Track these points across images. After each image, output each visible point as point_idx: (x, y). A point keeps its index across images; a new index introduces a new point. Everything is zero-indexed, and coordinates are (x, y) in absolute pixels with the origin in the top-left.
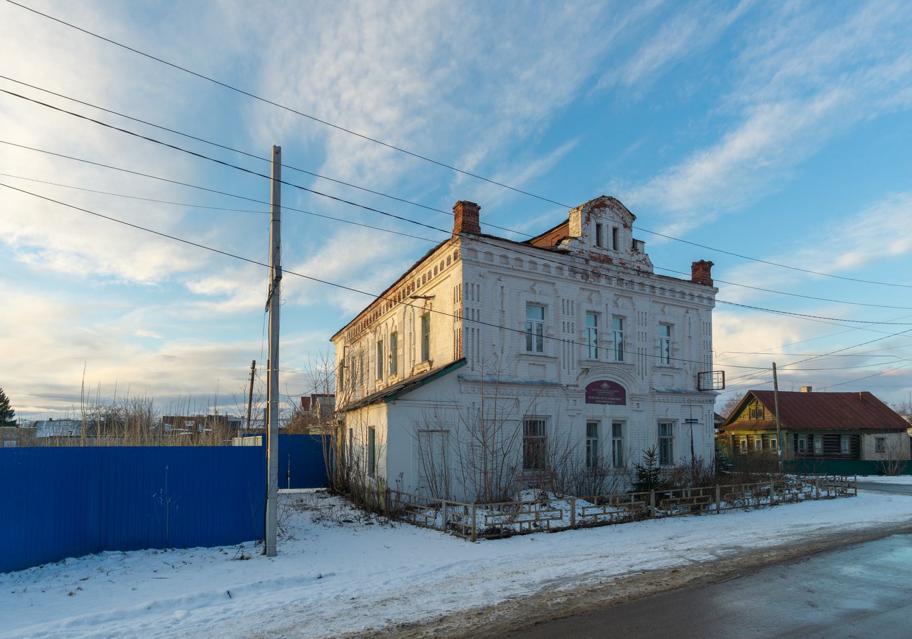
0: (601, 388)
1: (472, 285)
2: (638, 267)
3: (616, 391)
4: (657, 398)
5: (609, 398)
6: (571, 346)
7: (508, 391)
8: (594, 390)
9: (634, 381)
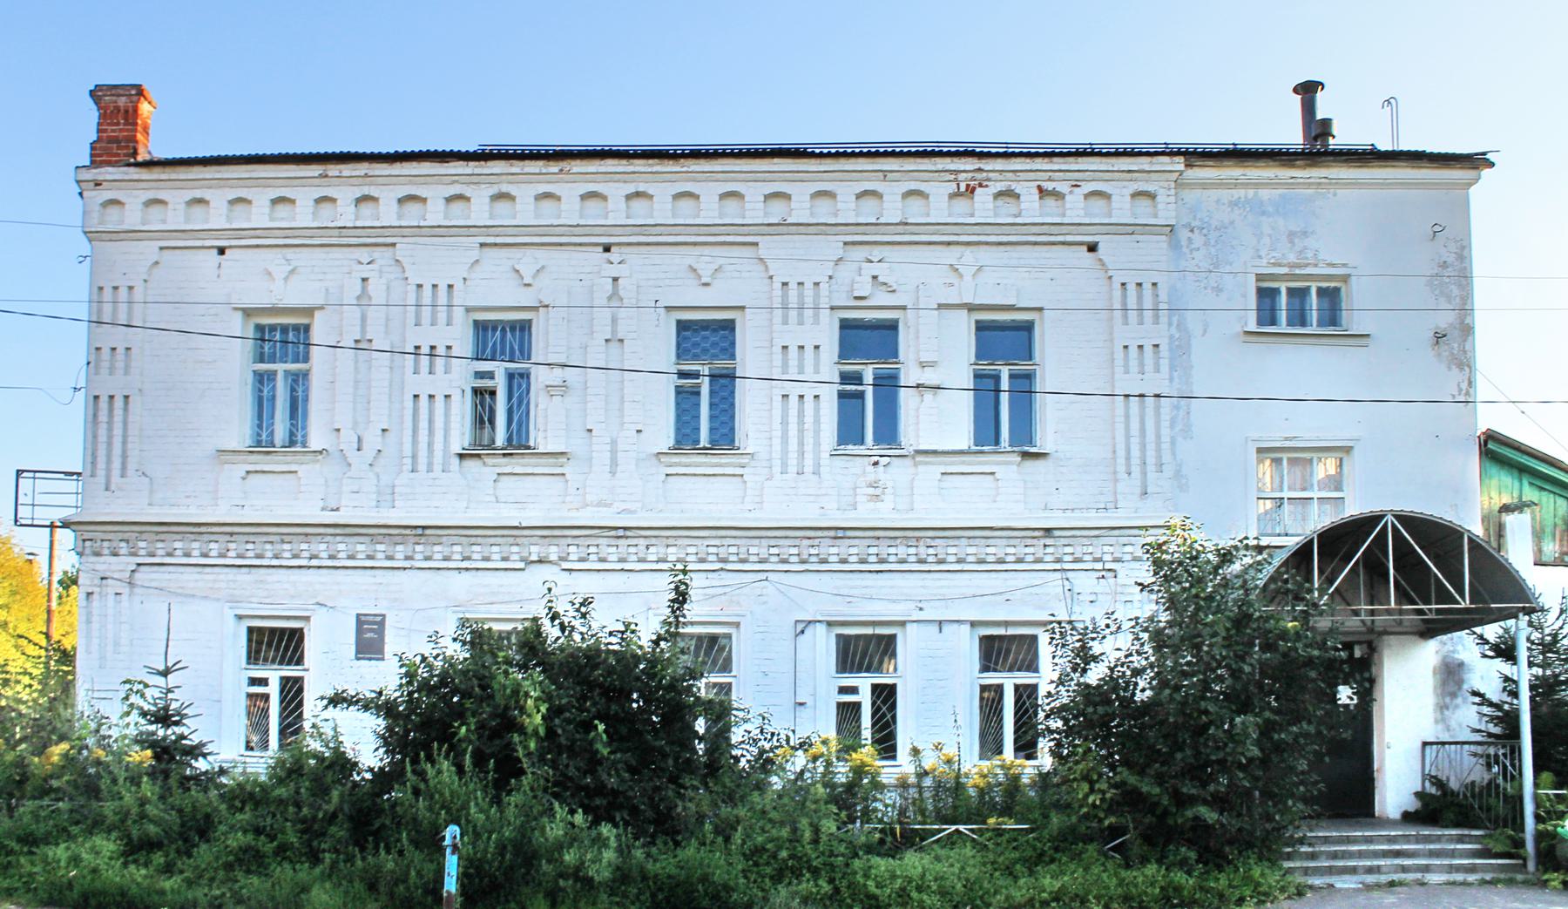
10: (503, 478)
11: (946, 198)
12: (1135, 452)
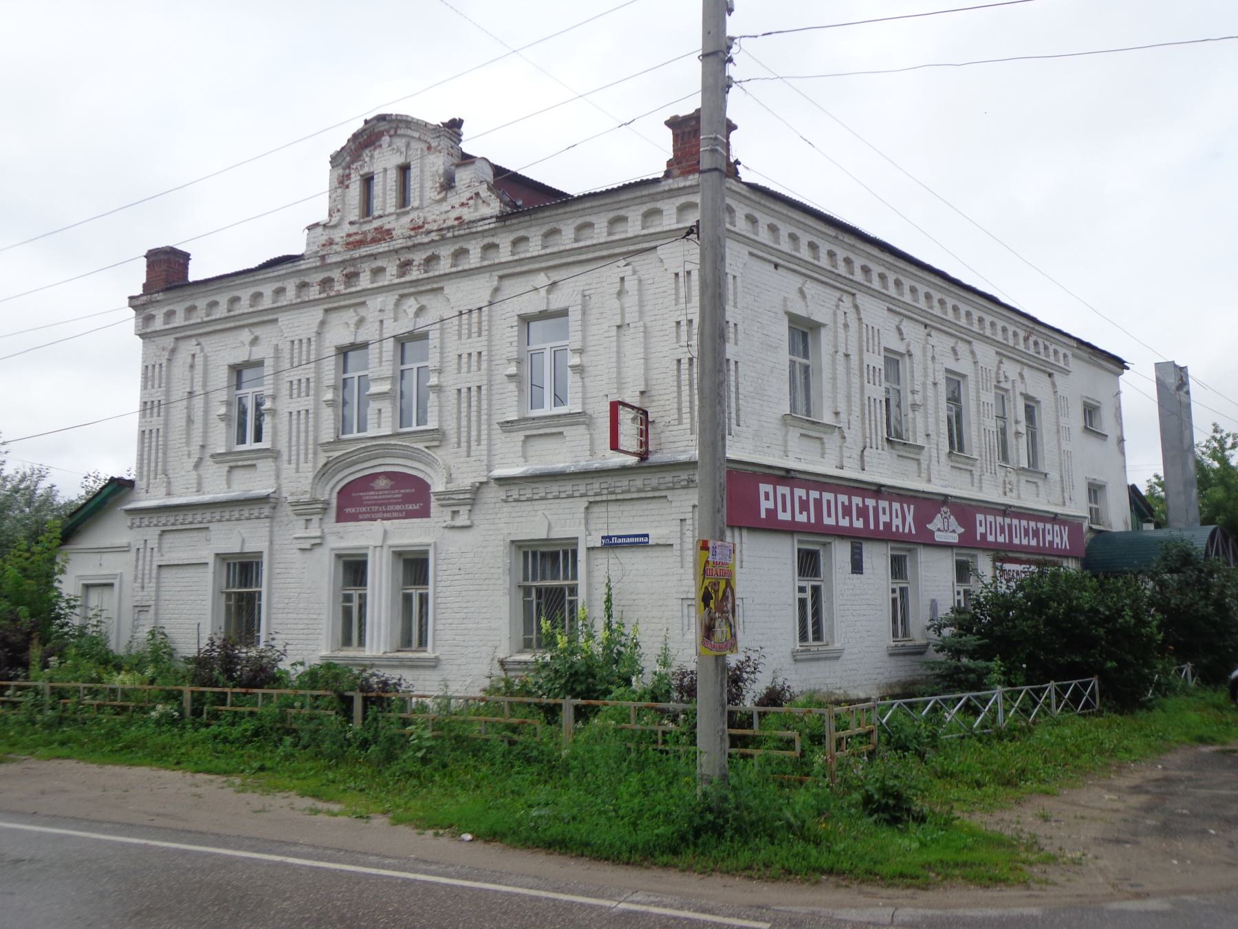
2: (458, 219)
3: (408, 491)
5: (391, 508)
7: (172, 520)
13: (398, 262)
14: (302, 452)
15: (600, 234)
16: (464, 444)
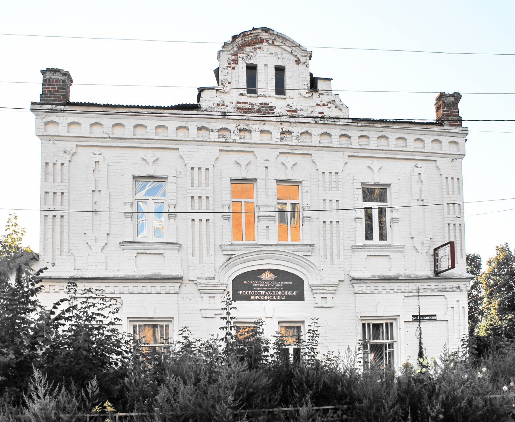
0: (260, 279)
1: (55, 164)
3: (287, 283)
4: (357, 287)
6: (198, 226)
8: (248, 282)
9: (313, 267)
10: (139, 255)
11: (89, 126)
12: (204, 240)
13: (281, 131)
14: (205, 249)
15: (128, 131)
16: (329, 257)
